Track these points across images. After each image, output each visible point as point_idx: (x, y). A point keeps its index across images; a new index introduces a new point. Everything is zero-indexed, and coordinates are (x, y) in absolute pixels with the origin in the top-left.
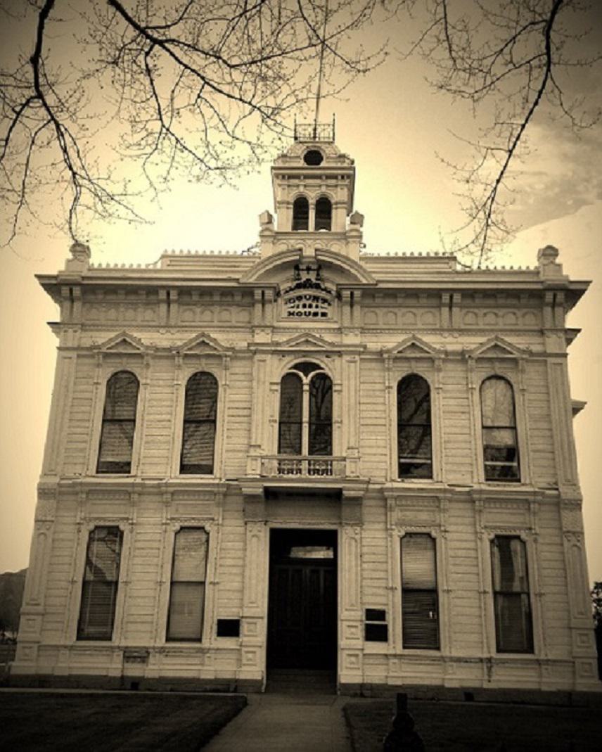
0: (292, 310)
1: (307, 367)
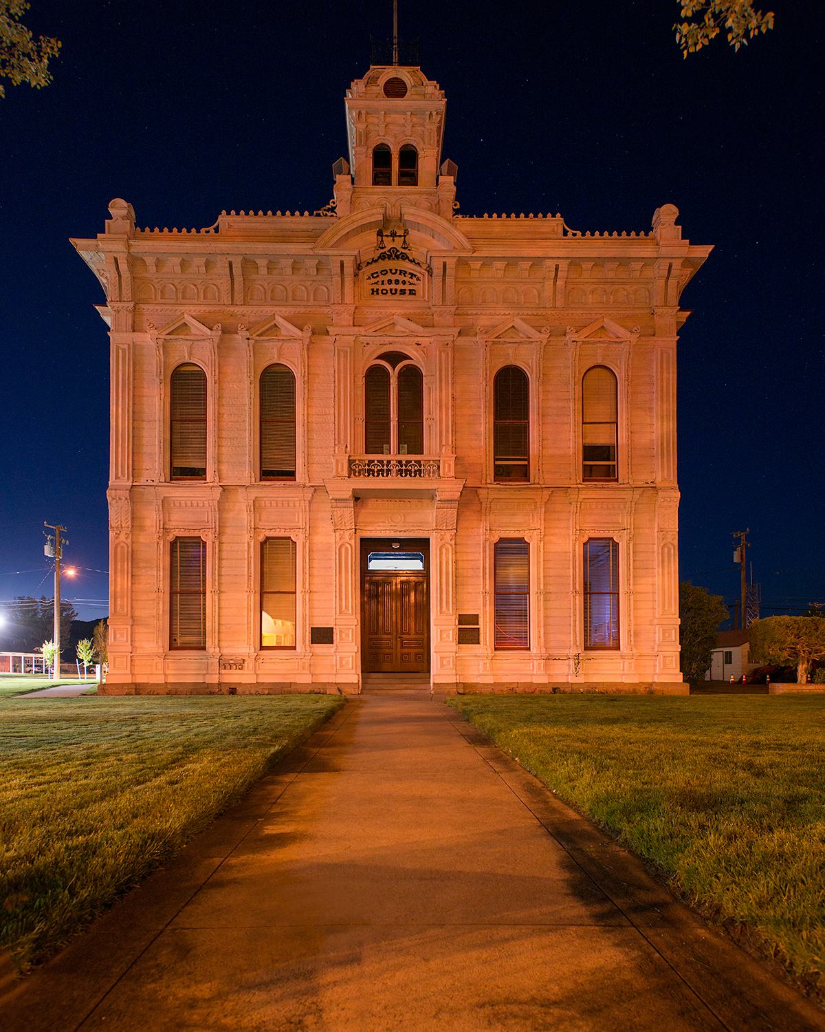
0: (375, 287)
1: (394, 357)
